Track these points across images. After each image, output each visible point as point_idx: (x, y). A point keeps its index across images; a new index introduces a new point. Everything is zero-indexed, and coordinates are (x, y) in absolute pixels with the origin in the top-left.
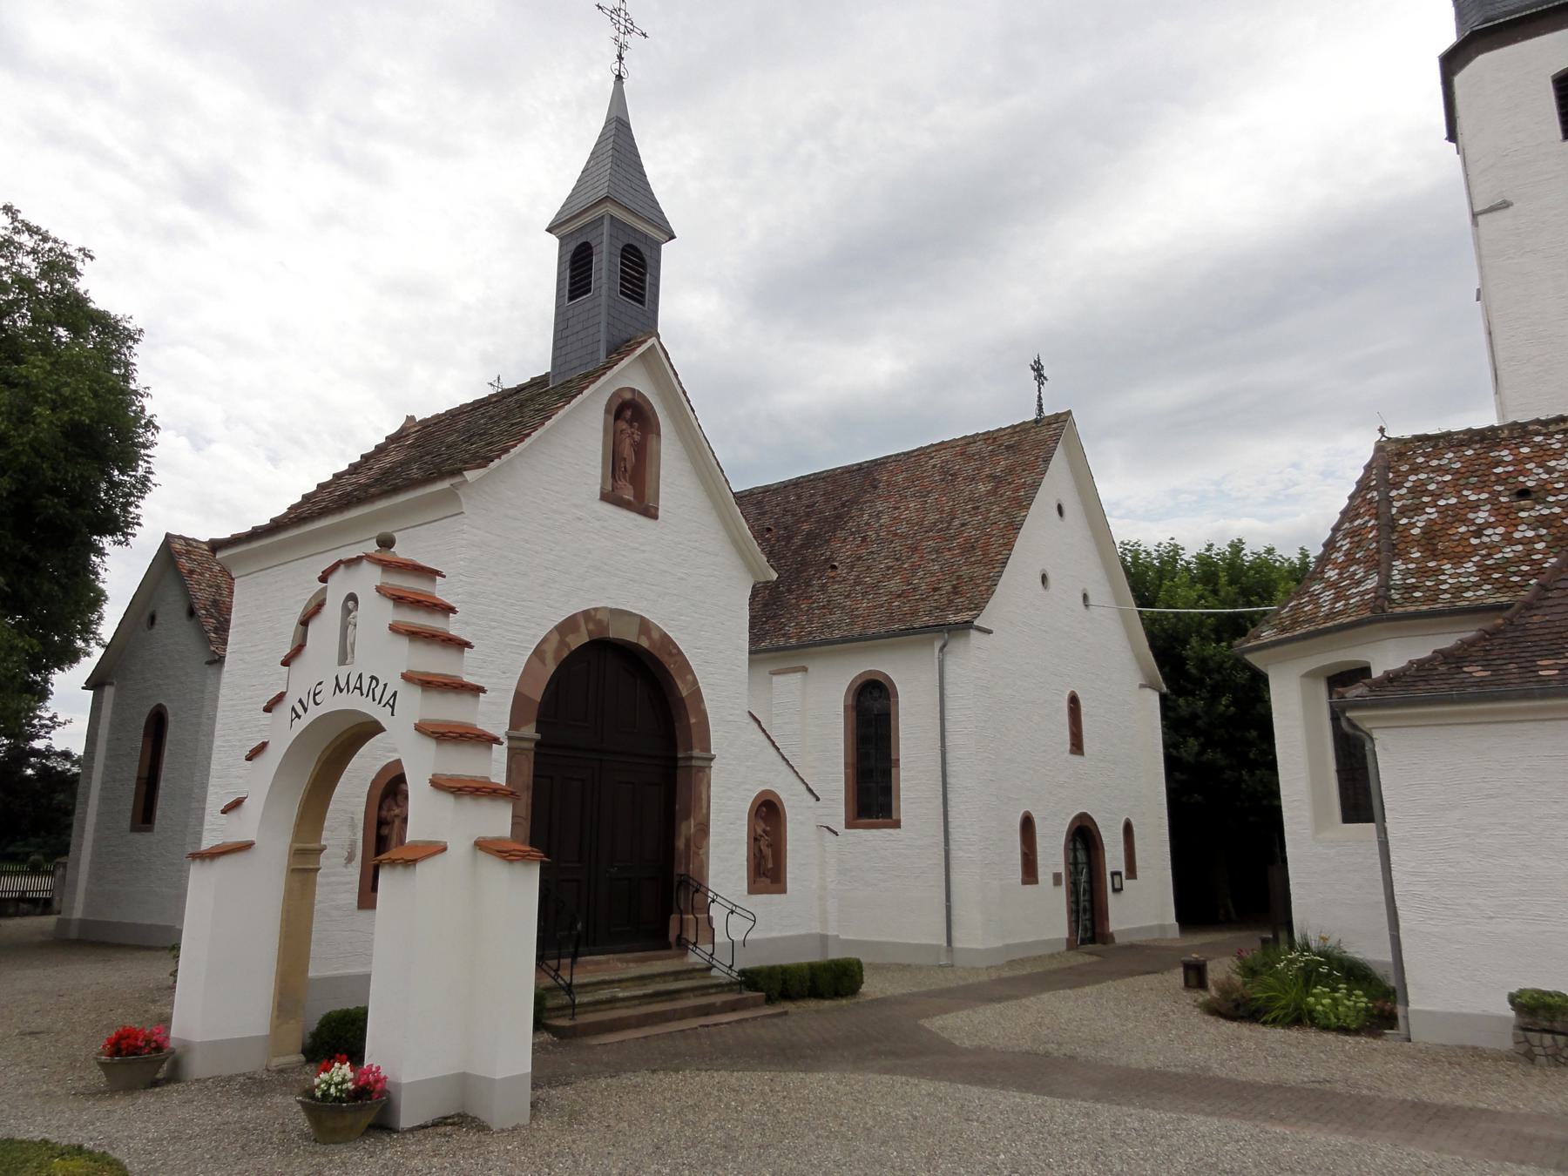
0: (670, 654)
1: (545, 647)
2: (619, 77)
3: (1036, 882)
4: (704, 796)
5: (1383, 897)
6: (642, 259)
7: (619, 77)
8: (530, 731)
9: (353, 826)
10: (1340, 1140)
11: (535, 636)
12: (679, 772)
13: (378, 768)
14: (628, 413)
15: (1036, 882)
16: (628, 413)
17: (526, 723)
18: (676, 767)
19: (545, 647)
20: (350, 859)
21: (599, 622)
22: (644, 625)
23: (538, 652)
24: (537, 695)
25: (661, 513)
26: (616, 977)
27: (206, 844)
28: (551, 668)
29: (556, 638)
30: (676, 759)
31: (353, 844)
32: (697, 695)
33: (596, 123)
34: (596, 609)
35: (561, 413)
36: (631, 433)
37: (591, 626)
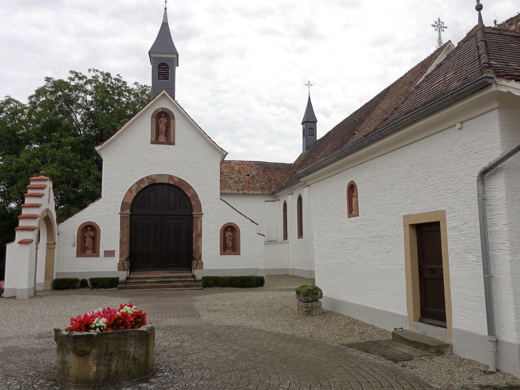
0: (183, 184)
1: (132, 189)
2: (166, 9)
3: (302, 238)
4: (199, 226)
5: (478, 224)
6: (167, 66)
7: (166, 9)
8: (128, 212)
9: (74, 238)
10: (436, 337)
11: (128, 186)
12: (194, 219)
13: (80, 224)
14: (163, 115)
15: (302, 238)
16: (163, 115)
17: (126, 209)
18: (193, 218)
19: (132, 189)
20: (74, 246)
21: (153, 179)
22: (171, 177)
23: (130, 190)
24: (130, 202)
25: (176, 143)
26: (156, 276)
27: (484, 331)
28: (135, 194)
29: (136, 185)
30: (192, 215)
31: (74, 242)
32: (196, 195)
33: (154, 31)
34: (151, 176)
35: (127, 124)
36: (163, 120)
37: (149, 181)
